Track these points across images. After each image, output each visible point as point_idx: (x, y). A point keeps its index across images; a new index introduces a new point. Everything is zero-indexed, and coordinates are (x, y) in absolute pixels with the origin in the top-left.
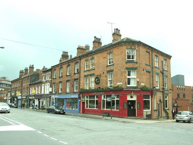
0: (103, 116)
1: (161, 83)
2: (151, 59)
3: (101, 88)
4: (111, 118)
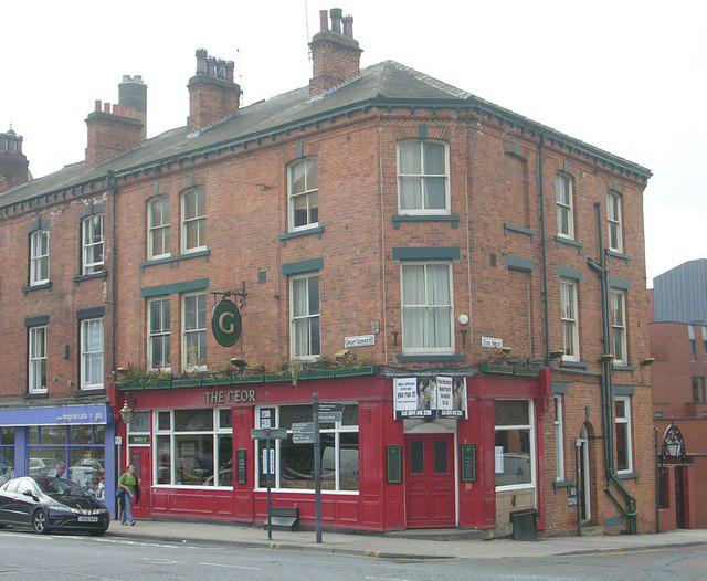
0: (270, 528)
1: (593, 332)
2: (532, 198)
3: (253, 364)
4: (319, 540)
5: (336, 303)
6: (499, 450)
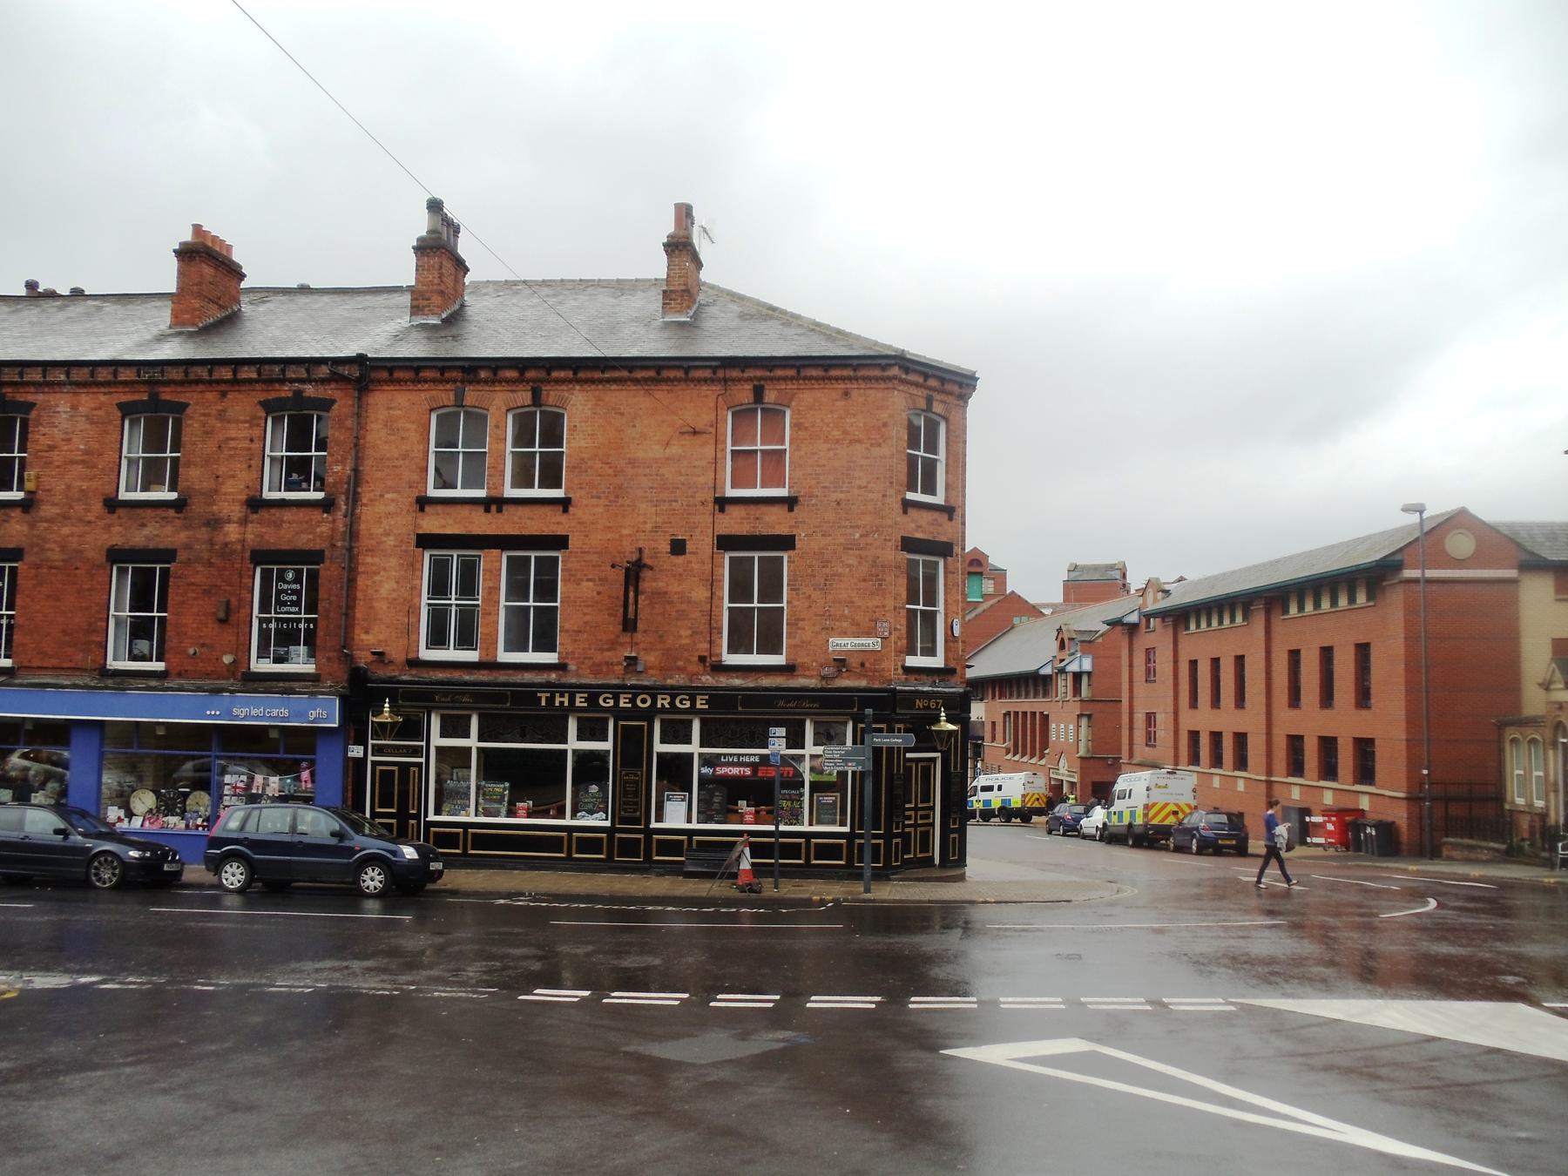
5: (816, 595)
6: (1504, 847)
